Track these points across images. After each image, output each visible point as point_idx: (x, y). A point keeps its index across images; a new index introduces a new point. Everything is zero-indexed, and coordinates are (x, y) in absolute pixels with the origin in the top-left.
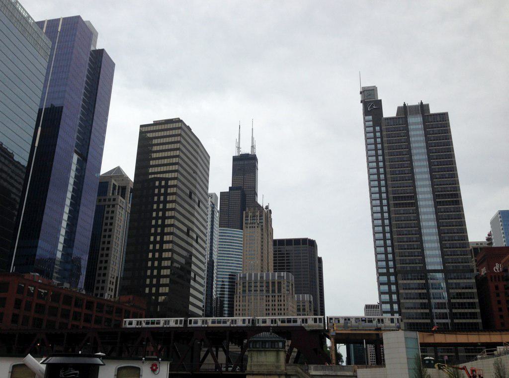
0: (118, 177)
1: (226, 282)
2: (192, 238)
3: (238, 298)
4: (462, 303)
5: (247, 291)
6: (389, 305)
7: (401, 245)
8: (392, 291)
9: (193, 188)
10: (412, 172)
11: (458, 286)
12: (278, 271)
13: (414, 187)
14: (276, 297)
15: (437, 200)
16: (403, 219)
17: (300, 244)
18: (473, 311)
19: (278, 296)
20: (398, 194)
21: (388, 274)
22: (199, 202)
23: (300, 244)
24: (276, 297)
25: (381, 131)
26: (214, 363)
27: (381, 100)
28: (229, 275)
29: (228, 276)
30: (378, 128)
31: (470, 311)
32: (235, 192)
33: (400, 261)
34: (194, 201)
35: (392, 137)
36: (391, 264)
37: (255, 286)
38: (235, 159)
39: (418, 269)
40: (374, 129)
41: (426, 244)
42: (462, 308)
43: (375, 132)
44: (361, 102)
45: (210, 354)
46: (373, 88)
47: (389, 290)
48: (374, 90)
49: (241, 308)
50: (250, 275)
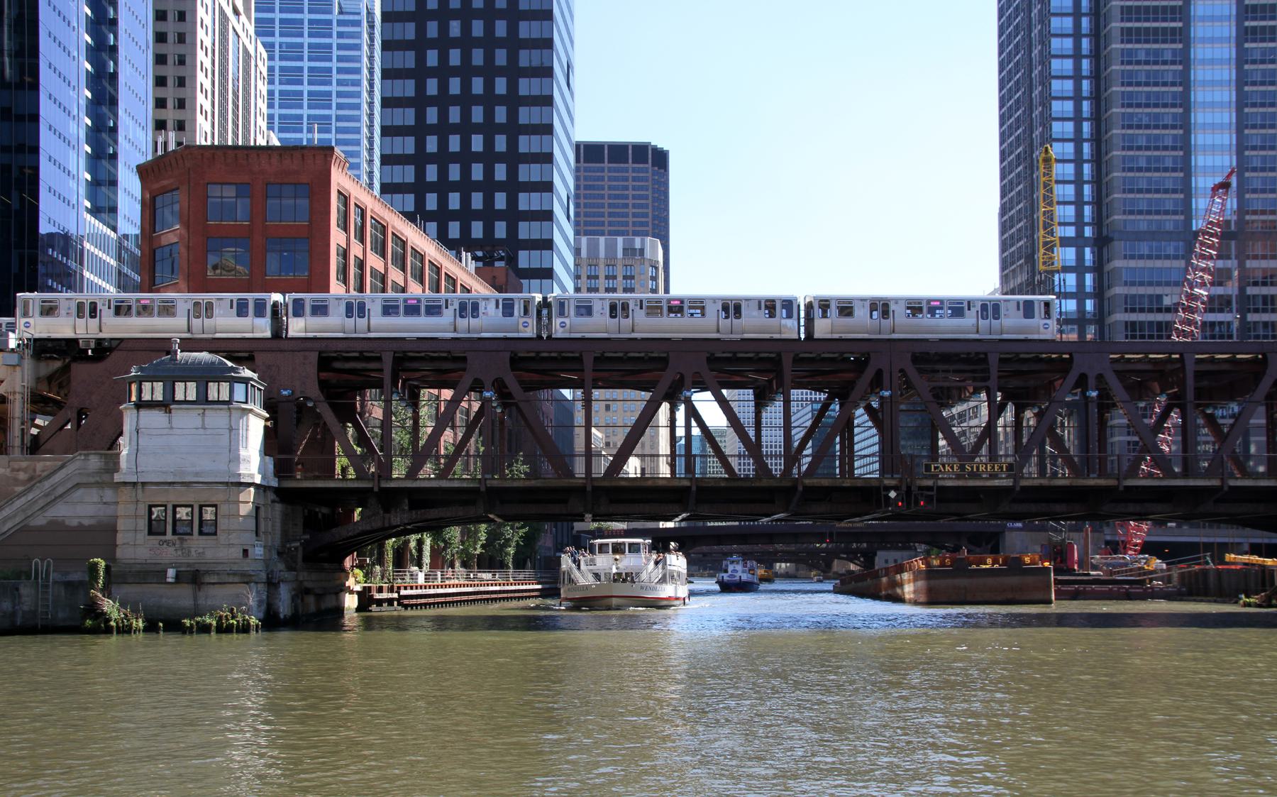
12: (606, 228)
15: (1247, 24)
17: (628, 163)
23: (628, 163)
33: (1124, 140)
39: (1169, 227)
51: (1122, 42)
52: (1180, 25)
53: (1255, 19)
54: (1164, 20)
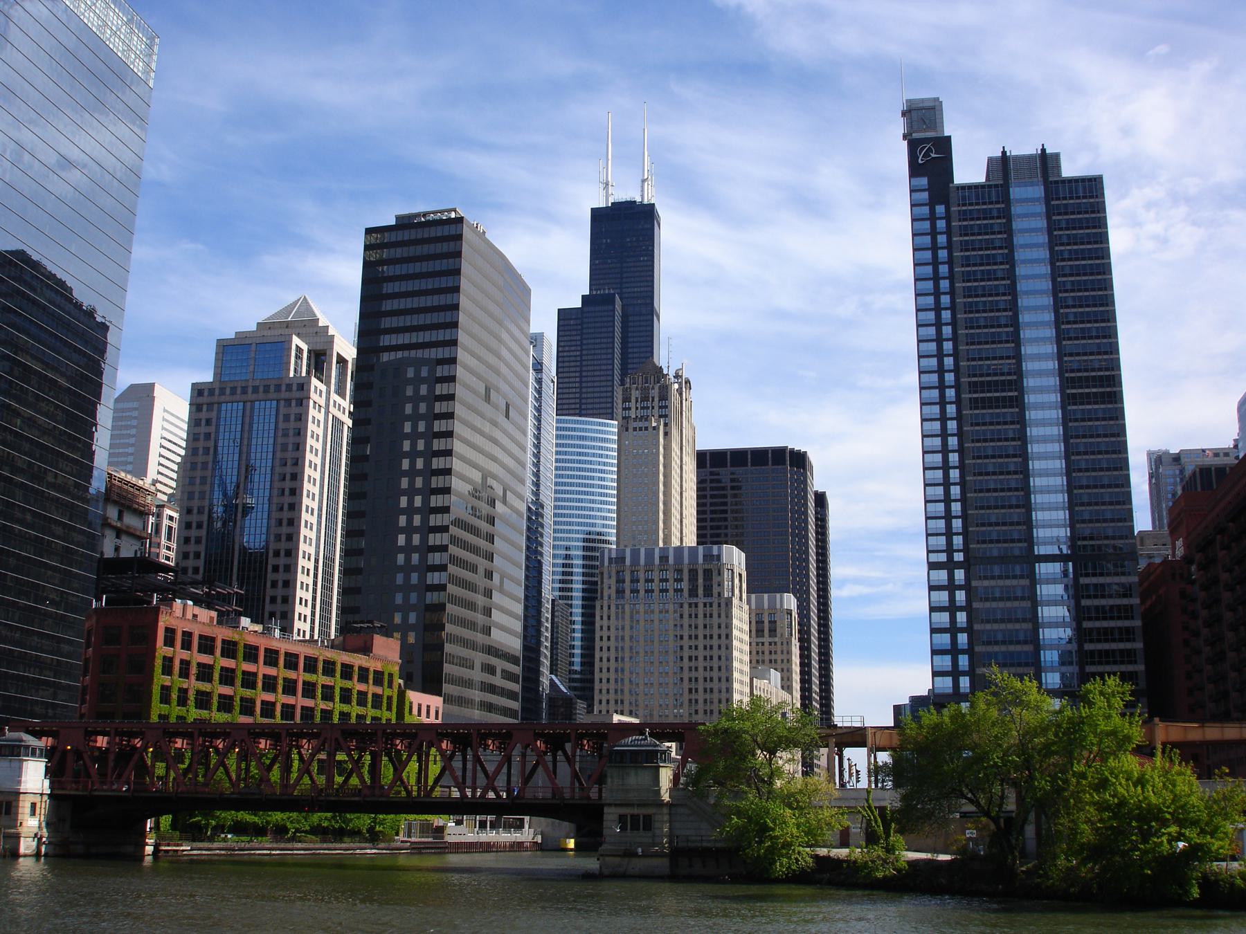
0: (304, 324)
1: (576, 548)
2: (496, 407)
3: (605, 608)
4: (1107, 652)
5: (628, 592)
6: (947, 614)
7: (968, 257)
8: (960, 647)
9: (493, 378)
10: (1015, 323)
11: (1100, 591)
13: (1018, 357)
14: (701, 606)
15: (1068, 391)
16: (982, 323)
18: (1128, 646)
19: (705, 605)
20: (981, 375)
21: (950, 566)
22: (508, 406)
24: (701, 606)
25: (948, 218)
26: (550, 785)
27: (949, 138)
28: (585, 540)
29: (581, 544)
30: (940, 209)
31: (1122, 646)
32: (597, 308)
34: (496, 407)
35: (972, 219)
36: (958, 541)
37: (647, 581)
38: (597, 214)
39: (1017, 552)
40: (932, 211)
41: (1033, 413)
42: (1106, 641)
43: (933, 218)
44: (905, 137)
45: (540, 766)
46: (932, 104)
47: (935, 303)
48: (933, 108)
49: (613, 633)
50: (635, 553)
51: (971, 409)
52: (1016, 394)
53: (1074, 388)
54: (983, 392)
